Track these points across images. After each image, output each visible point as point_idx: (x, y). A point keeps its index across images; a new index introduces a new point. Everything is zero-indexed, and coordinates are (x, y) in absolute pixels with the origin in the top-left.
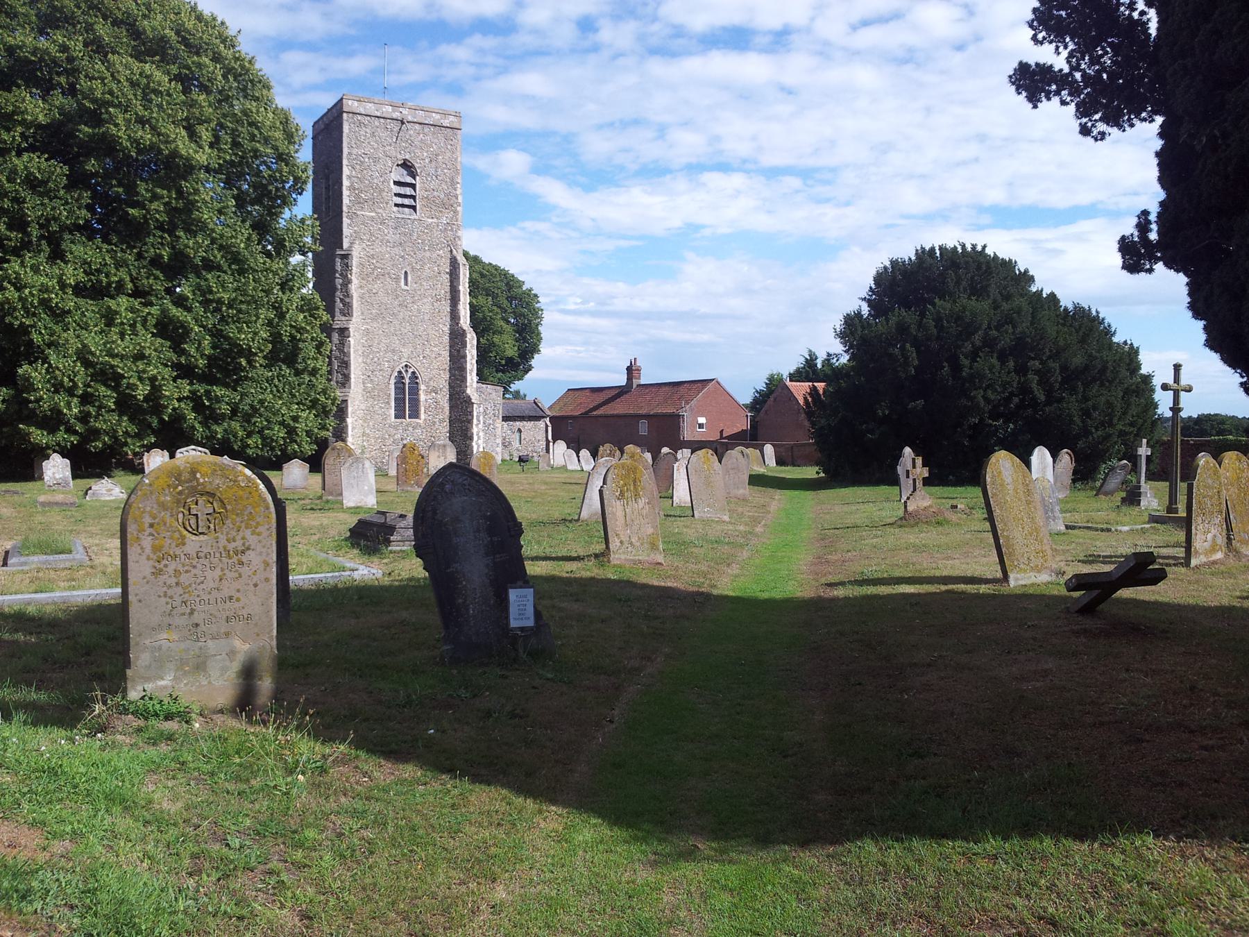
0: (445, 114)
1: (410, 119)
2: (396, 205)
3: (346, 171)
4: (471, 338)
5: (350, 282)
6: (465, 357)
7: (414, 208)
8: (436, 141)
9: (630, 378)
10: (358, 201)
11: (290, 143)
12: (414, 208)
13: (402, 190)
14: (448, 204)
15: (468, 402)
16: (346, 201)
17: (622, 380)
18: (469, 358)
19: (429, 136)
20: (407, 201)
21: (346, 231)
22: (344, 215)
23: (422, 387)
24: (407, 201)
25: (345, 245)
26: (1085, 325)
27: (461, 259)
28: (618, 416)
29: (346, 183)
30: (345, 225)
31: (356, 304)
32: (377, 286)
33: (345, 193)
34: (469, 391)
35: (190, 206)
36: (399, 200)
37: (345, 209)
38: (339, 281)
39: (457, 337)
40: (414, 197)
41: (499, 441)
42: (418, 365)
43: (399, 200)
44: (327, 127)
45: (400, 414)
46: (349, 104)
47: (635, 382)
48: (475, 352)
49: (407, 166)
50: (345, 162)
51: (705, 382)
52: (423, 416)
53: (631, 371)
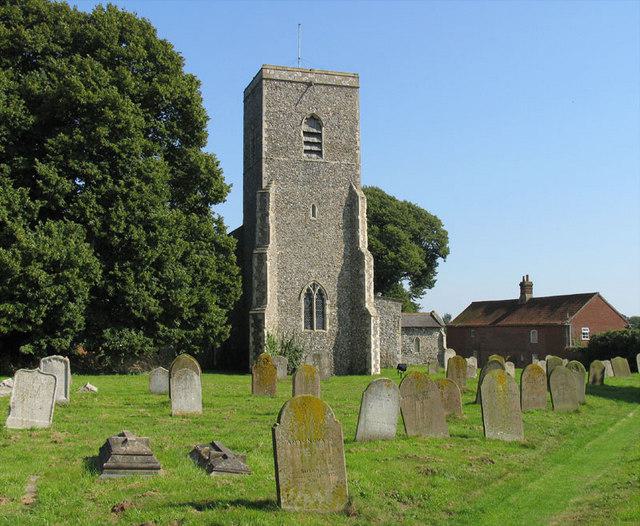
0: (346, 77)
1: (317, 81)
2: (306, 151)
3: (265, 125)
4: (369, 262)
5: (268, 215)
6: (363, 276)
7: (319, 153)
8: (338, 97)
9: (523, 293)
10: (274, 150)
11: (228, 292)
12: (319, 153)
13: (311, 139)
14: (350, 149)
15: (366, 315)
16: (265, 149)
17: (514, 294)
18: (366, 277)
19: (333, 94)
20: (315, 148)
21: (265, 174)
22: (264, 160)
23: (328, 302)
24: (315, 148)
25: (264, 186)
26: (362, 254)
27: (360, 194)
28: (512, 326)
29: (265, 135)
30: (264, 169)
31: (272, 233)
32: (289, 218)
33: (265, 142)
34: (367, 306)
35: (90, 106)
36: (308, 148)
37: (264, 156)
38: (259, 215)
39: (354, 259)
40: (319, 144)
41: (399, 348)
42: (323, 283)
43: (308, 148)
44: (253, 91)
45: (310, 324)
46: (267, 73)
47: (528, 296)
48: (372, 272)
49: (314, 120)
50: (264, 118)
51: (590, 296)
52: (328, 327)
53: (525, 286)
